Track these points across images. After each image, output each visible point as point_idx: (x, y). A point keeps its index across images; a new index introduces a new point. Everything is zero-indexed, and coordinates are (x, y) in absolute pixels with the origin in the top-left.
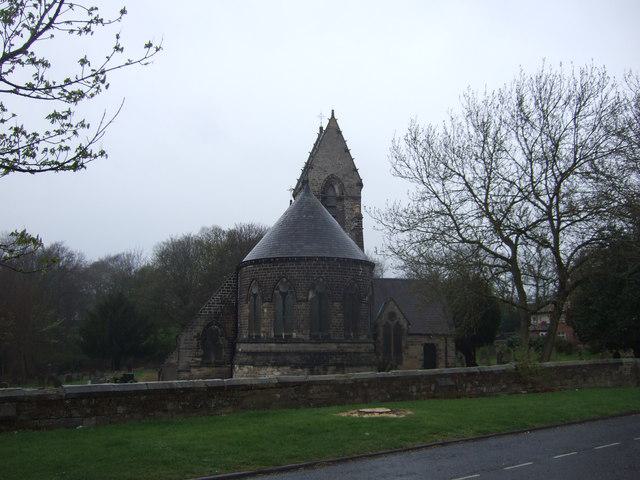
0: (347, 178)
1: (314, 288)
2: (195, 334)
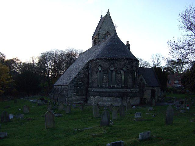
2: (74, 84)
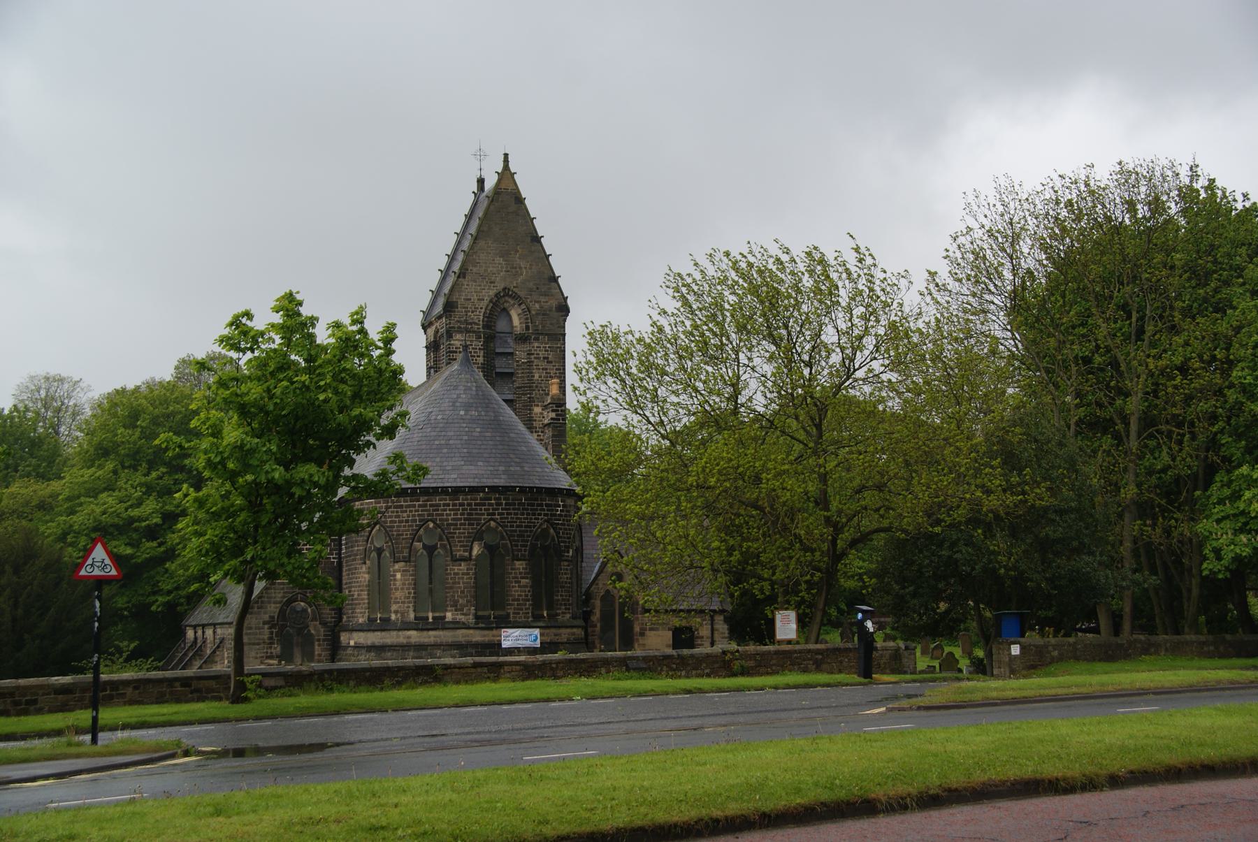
1: (481, 539)
2: (266, 617)
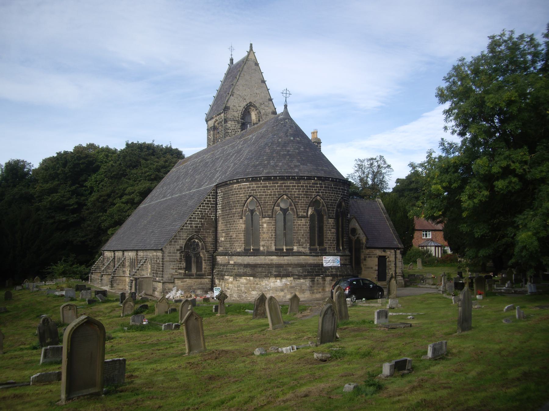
0: (263, 106)
2: (178, 247)
